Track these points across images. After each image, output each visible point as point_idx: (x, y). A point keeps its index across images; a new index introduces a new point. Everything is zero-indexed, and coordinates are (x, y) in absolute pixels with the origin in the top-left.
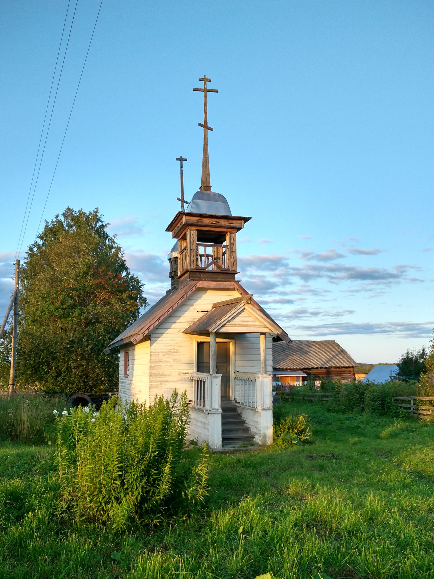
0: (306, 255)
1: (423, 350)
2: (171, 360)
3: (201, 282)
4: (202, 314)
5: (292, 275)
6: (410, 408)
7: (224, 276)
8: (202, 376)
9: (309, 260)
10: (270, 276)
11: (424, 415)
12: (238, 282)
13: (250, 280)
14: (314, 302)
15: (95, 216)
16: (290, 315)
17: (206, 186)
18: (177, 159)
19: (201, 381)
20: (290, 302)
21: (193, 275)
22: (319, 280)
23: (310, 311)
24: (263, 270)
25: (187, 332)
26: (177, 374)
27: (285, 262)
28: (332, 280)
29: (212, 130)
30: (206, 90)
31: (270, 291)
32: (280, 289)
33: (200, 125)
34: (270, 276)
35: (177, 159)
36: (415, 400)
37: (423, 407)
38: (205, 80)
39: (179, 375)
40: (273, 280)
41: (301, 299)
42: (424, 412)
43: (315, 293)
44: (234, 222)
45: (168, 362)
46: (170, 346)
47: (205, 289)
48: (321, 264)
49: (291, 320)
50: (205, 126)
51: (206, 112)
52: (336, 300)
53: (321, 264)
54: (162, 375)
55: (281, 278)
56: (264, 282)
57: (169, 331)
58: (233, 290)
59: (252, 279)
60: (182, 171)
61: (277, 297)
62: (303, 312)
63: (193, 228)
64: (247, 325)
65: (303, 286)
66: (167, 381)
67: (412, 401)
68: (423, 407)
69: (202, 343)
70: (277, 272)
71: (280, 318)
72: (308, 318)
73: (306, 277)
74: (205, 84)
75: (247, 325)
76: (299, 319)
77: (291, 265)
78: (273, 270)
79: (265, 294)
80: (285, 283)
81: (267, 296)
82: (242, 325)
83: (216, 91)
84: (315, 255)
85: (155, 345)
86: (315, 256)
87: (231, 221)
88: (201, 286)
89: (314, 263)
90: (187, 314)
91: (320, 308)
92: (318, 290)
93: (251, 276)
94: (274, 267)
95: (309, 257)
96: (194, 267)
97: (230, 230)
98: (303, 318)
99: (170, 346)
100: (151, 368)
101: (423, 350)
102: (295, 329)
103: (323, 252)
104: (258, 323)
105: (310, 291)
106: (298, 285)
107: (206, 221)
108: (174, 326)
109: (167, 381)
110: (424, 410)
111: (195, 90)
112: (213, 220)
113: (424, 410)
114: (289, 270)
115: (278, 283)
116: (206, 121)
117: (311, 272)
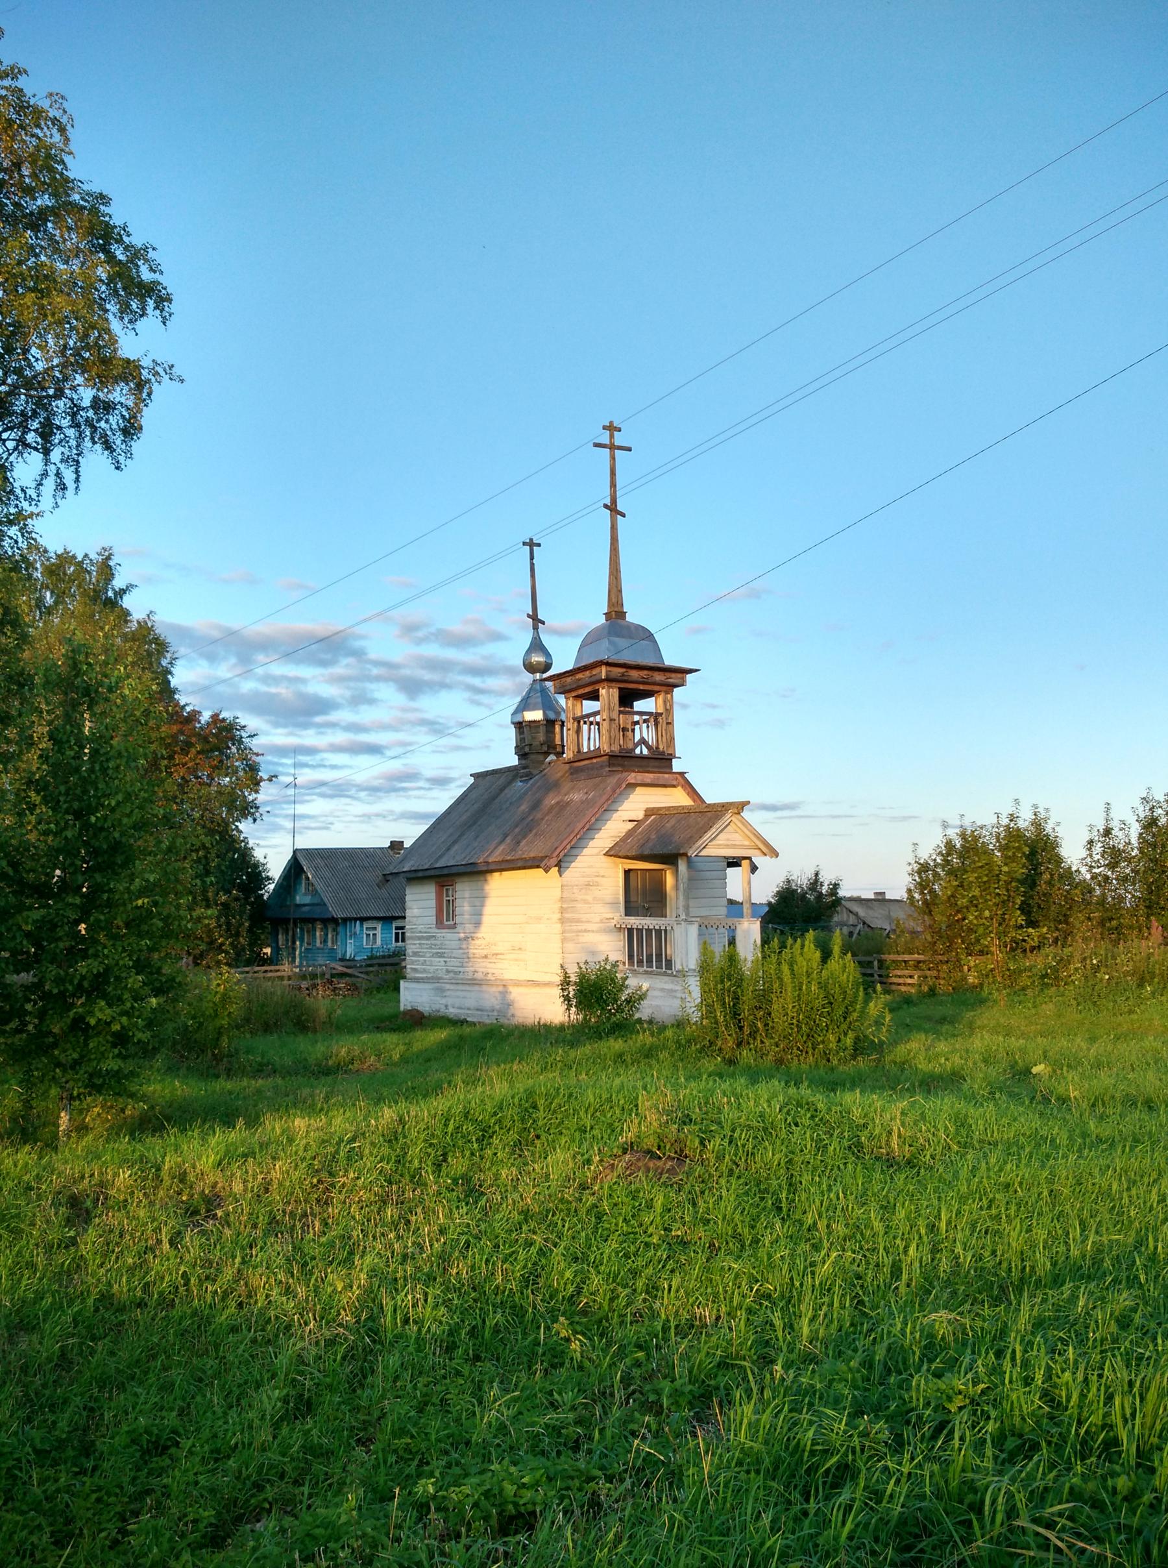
0: (409, 629)
1: (817, 874)
2: (589, 898)
3: (633, 775)
4: (631, 825)
5: (378, 679)
6: (872, 975)
7: (657, 763)
8: (638, 922)
9: (420, 641)
10: (317, 681)
11: (899, 984)
12: (682, 774)
13: (264, 688)
14: (433, 752)
15: (106, 570)
16: (376, 783)
17: (616, 613)
18: (524, 544)
19: (660, 930)
20: (374, 749)
21: (614, 761)
22: (444, 695)
23: (429, 773)
24: (299, 662)
25: (612, 853)
26: (598, 920)
27: (358, 644)
28: (477, 697)
29: (623, 515)
30: (612, 447)
31: (318, 719)
32: (343, 715)
33: (606, 506)
34: (317, 681)
35: (524, 544)
36: (881, 962)
37: (899, 973)
38: (611, 428)
39: (601, 922)
40: (327, 691)
41: (403, 744)
42: (901, 981)
43: (435, 727)
44: (673, 675)
45: (586, 902)
46: (588, 876)
47: (635, 785)
48: (451, 654)
49: (380, 798)
50: (613, 508)
51: (613, 485)
52: (488, 747)
53: (451, 654)
54: (578, 921)
55: (348, 688)
56: (302, 696)
57: (585, 851)
58: (674, 786)
59: (268, 685)
60: (532, 565)
61: (340, 737)
62: (411, 776)
63: (613, 684)
64: (734, 846)
65: (404, 710)
66: (586, 931)
67: (876, 963)
68: (899, 973)
69: (630, 870)
70: (338, 670)
71: (352, 792)
72: (422, 792)
73: (412, 687)
74: (612, 436)
75: (734, 846)
76: (401, 793)
77: (373, 655)
78: (323, 663)
79: (306, 726)
80: (360, 700)
81: (311, 732)
82: (727, 847)
83: (629, 449)
84: (433, 630)
85: (567, 874)
86: (432, 634)
87: (668, 675)
88: (633, 781)
89: (432, 650)
90: (609, 825)
91: (451, 768)
92: (441, 721)
93: (268, 679)
94: (328, 656)
95: (420, 634)
96: (616, 748)
97: (664, 688)
98: (411, 793)
99: (588, 876)
100: (562, 910)
101: (817, 874)
102: (395, 820)
103: (455, 626)
104: (747, 843)
105: (423, 722)
106: (391, 708)
107: (634, 674)
108: (592, 844)
109: (586, 931)
110: (900, 977)
111: (597, 445)
112: (644, 673)
113: (900, 977)
114: (368, 666)
115: (339, 700)
116: (614, 501)
117: (427, 676)
